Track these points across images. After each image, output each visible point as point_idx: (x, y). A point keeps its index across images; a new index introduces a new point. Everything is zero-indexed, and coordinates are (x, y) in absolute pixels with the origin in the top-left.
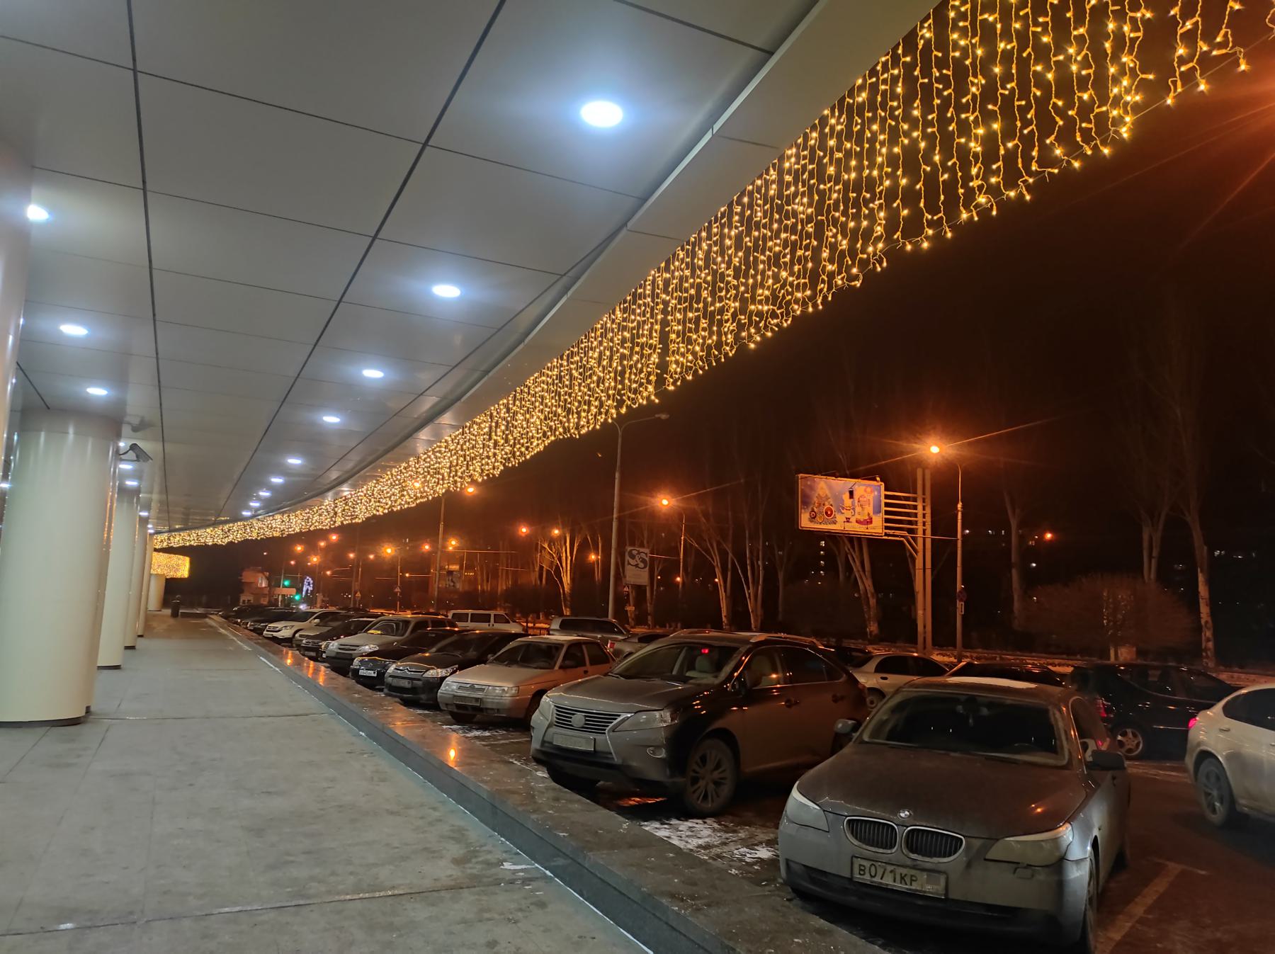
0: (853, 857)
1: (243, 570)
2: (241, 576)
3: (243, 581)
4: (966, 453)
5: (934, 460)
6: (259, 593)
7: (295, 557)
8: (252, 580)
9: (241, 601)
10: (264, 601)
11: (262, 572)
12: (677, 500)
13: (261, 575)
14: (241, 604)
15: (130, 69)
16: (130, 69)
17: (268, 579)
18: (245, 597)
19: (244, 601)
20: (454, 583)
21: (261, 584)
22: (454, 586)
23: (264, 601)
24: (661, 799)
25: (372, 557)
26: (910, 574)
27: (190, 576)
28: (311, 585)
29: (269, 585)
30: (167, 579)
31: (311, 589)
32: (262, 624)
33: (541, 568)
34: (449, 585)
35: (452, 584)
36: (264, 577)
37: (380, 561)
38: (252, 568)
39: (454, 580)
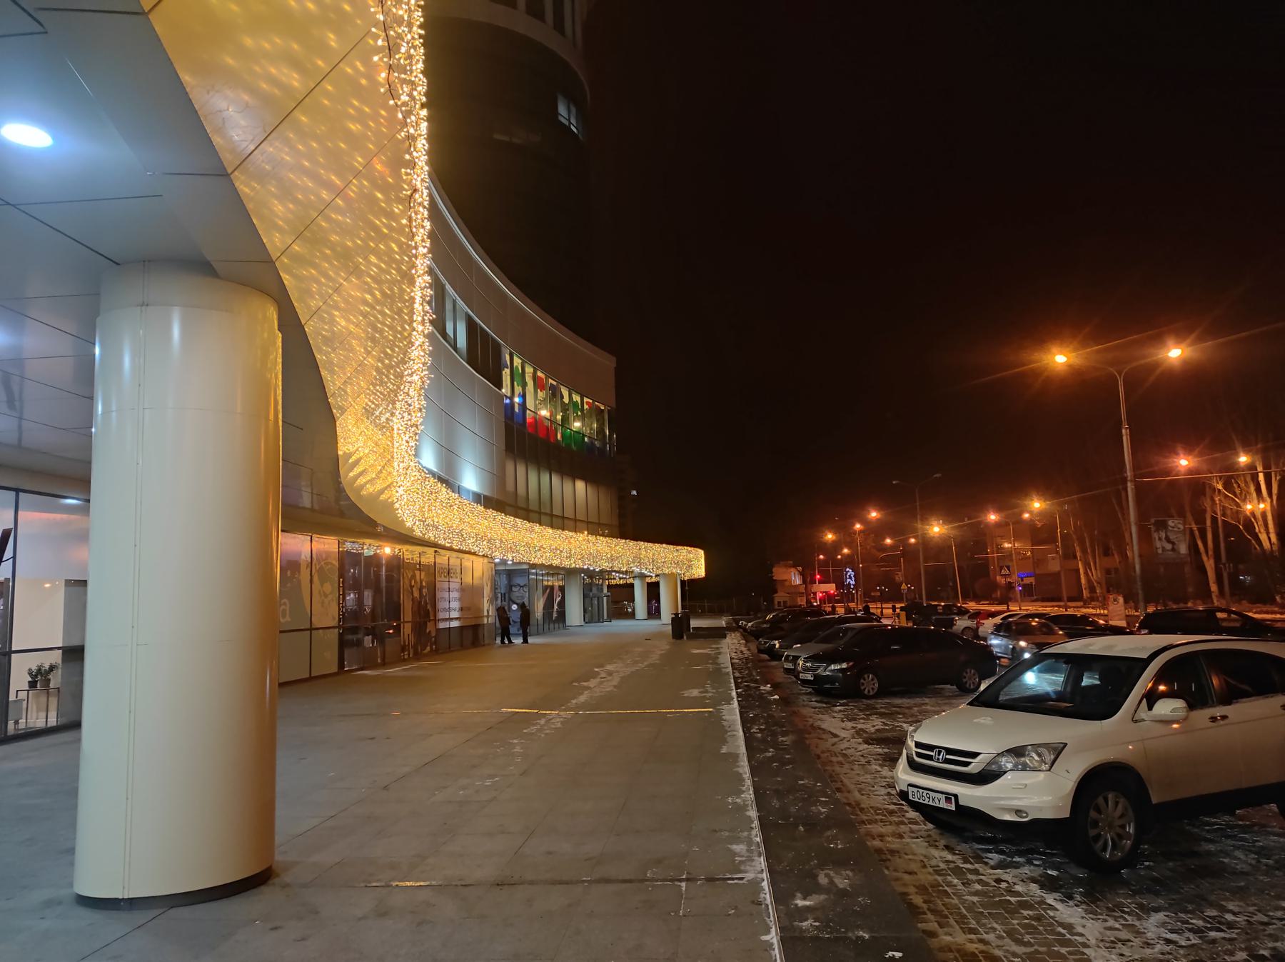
0: (17, 691)
1: (773, 566)
2: (772, 573)
3: (774, 578)
4: (953, 533)
5: (1037, 510)
6: (794, 591)
7: (824, 548)
8: (785, 577)
9: (776, 603)
10: (801, 601)
11: (795, 566)
12: (1047, 504)
13: (793, 570)
14: (776, 607)
15: (311, 634)
16: (311, 634)
17: (802, 574)
18: (780, 597)
19: (779, 603)
20: (1173, 543)
21: (795, 581)
22: (1173, 550)
23: (802, 602)
24: (608, 434)
25: (839, 557)
26: (1213, 632)
27: (706, 575)
28: (853, 579)
29: (804, 581)
30: (683, 582)
31: (854, 583)
32: (833, 667)
33: (1214, 520)
34: (1163, 548)
35: (1169, 546)
36: (797, 573)
37: (926, 542)
38: (781, 563)
39: (1172, 537)
